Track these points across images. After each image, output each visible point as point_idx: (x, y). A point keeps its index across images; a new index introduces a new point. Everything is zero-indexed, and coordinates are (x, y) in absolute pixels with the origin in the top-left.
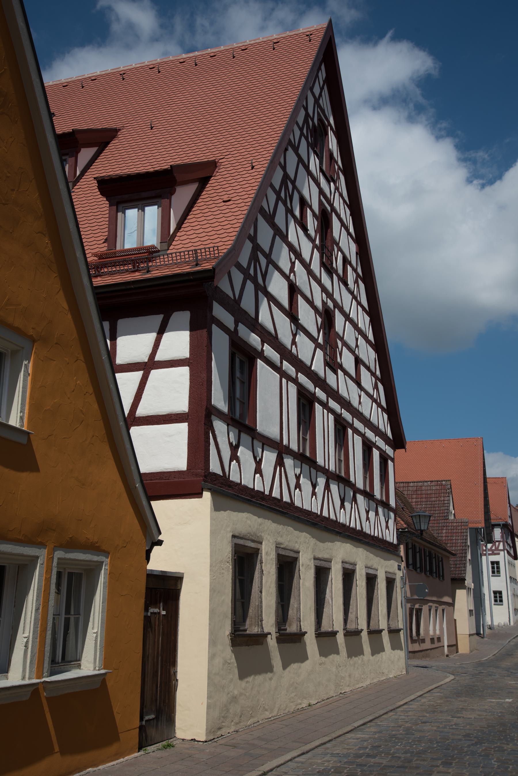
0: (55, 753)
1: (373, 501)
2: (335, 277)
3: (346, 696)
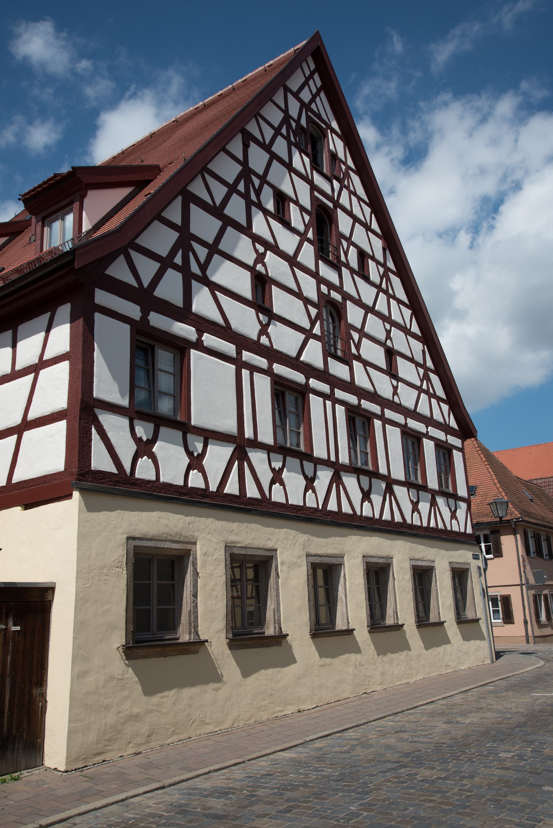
2: (344, 270)
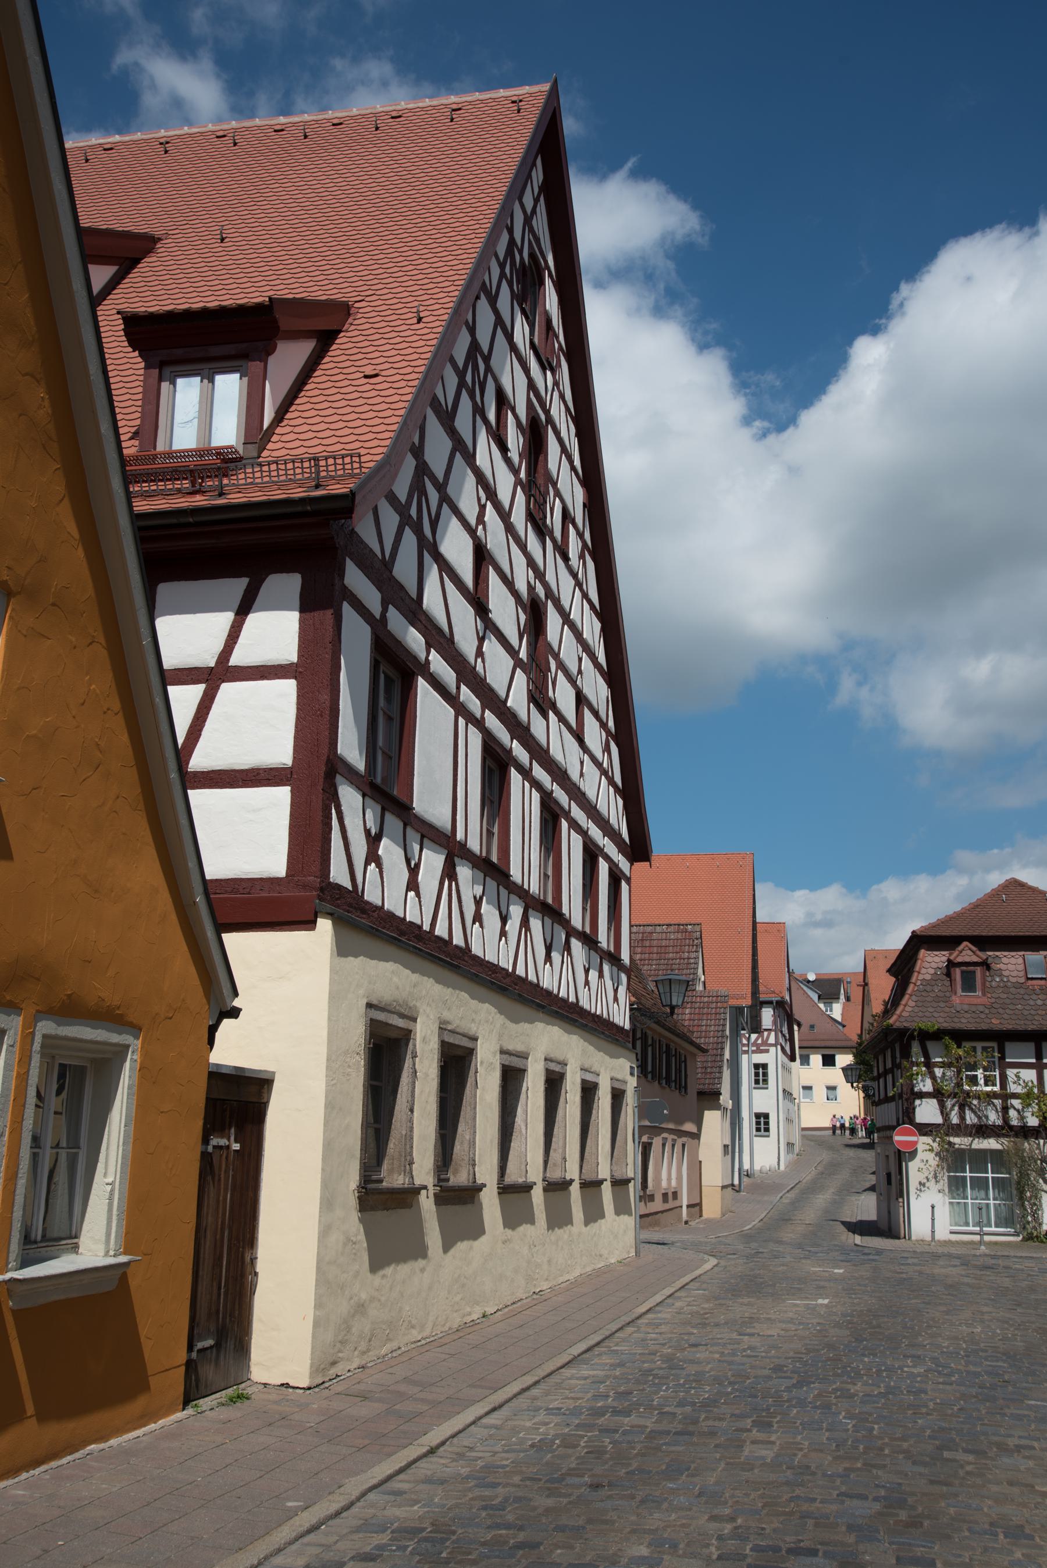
0: (27, 1418)
1: (596, 952)
3: (544, 1297)
